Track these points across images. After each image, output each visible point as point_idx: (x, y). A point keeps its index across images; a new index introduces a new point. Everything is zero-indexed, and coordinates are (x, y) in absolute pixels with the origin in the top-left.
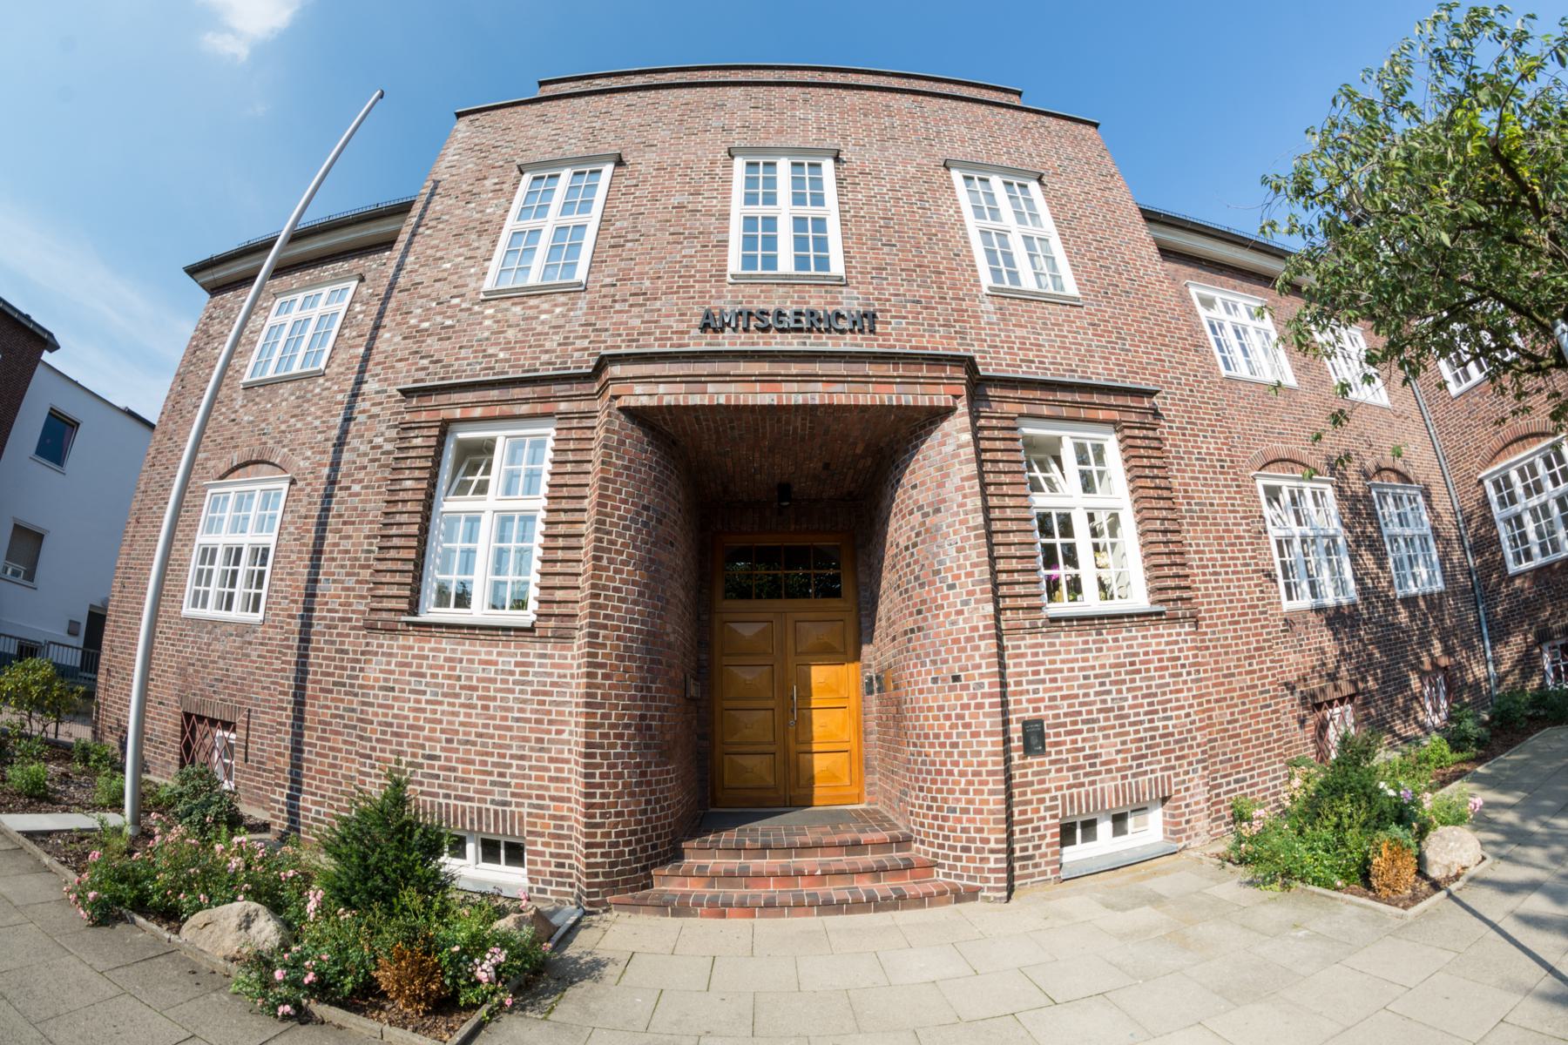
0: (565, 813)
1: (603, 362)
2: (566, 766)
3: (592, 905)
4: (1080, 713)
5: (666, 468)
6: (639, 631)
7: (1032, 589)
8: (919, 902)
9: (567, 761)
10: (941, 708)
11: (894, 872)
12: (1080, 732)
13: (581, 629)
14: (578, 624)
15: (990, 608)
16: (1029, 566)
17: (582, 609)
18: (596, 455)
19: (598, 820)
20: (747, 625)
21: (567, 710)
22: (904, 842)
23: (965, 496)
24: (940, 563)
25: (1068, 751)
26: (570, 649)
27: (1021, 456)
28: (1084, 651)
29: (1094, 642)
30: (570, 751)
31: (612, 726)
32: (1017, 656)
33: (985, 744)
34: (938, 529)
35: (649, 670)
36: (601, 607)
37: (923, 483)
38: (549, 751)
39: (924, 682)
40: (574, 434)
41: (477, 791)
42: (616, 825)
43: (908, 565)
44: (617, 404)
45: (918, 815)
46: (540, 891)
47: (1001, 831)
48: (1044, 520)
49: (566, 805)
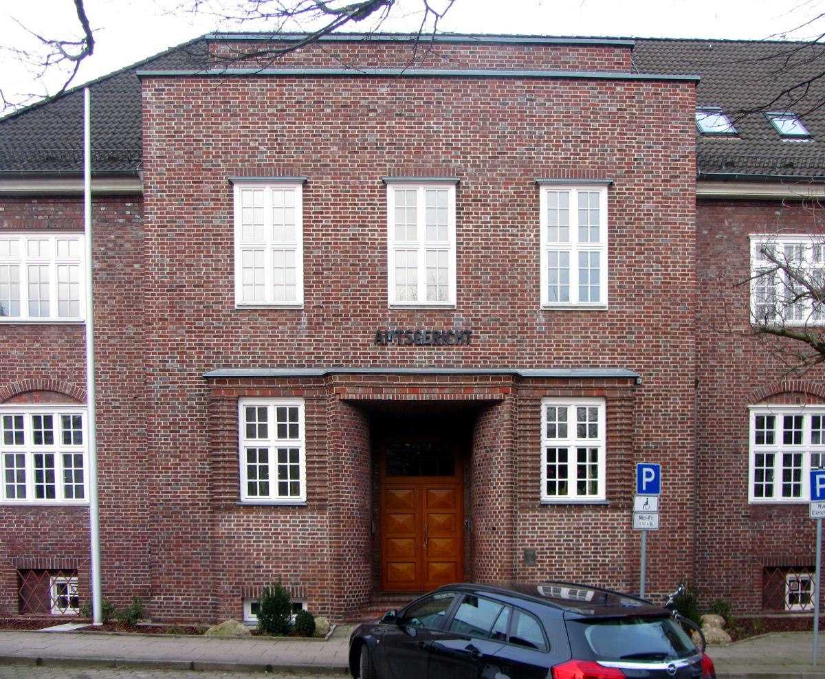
10: (488, 541)
31: (347, 547)
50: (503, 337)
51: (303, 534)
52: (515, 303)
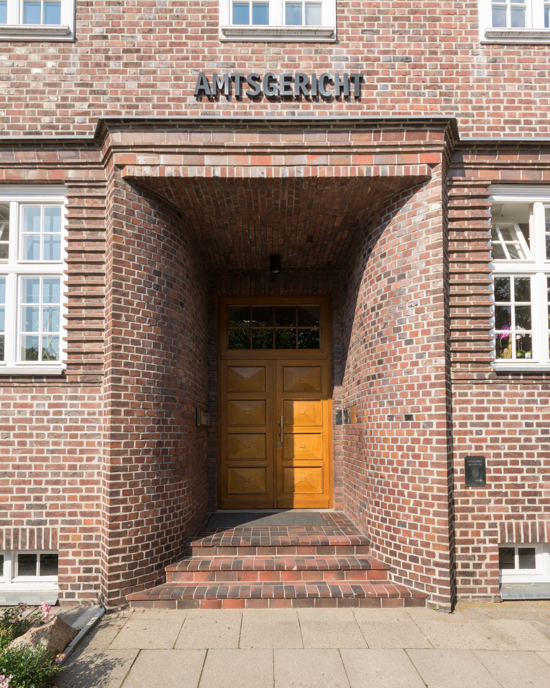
0: (94, 526)
1: (105, 126)
2: (96, 487)
3: (113, 603)
4: (521, 455)
5: (173, 238)
6: (156, 376)
7: (482, 346)
8: (376, 601)
9: (97, 482)
10: (395, 440)
11: (356, 575)
12: (520, 471)
13: (106, 375)
14: (103, 371)
15: (442, 361)
16: (482, 326)
17: (106, 359)
18: (108, 224)
19: (121, 530)
20: (246, 369)
21: (96, 441)
22: (362, 545)
23: (428, 263)
24: (401, 322)
25: (507, 486)
26: (98, 391)
27: (488, 224)
28: (528, 402)
29: (539, 395)
30: (99, 474)
31: (133, 452)
32: (464, 402)
33: (432, 473)
34: (401, 292)
35: (165, 407)
36: (121, 357)
37: (391, 252)
38: (81, 475)
39: (382, 418)
40: (86, 203)
41: (14, 515)
42: (136, 532)
43: (373, 323)
44: (123, 173)
45: (374, 525)
46: (69, 595)
47: (444, 548)
48: (502, 284)
49: (95, 519)
50: (417, 88)
51: (56, 428)
52: (436, 33)
